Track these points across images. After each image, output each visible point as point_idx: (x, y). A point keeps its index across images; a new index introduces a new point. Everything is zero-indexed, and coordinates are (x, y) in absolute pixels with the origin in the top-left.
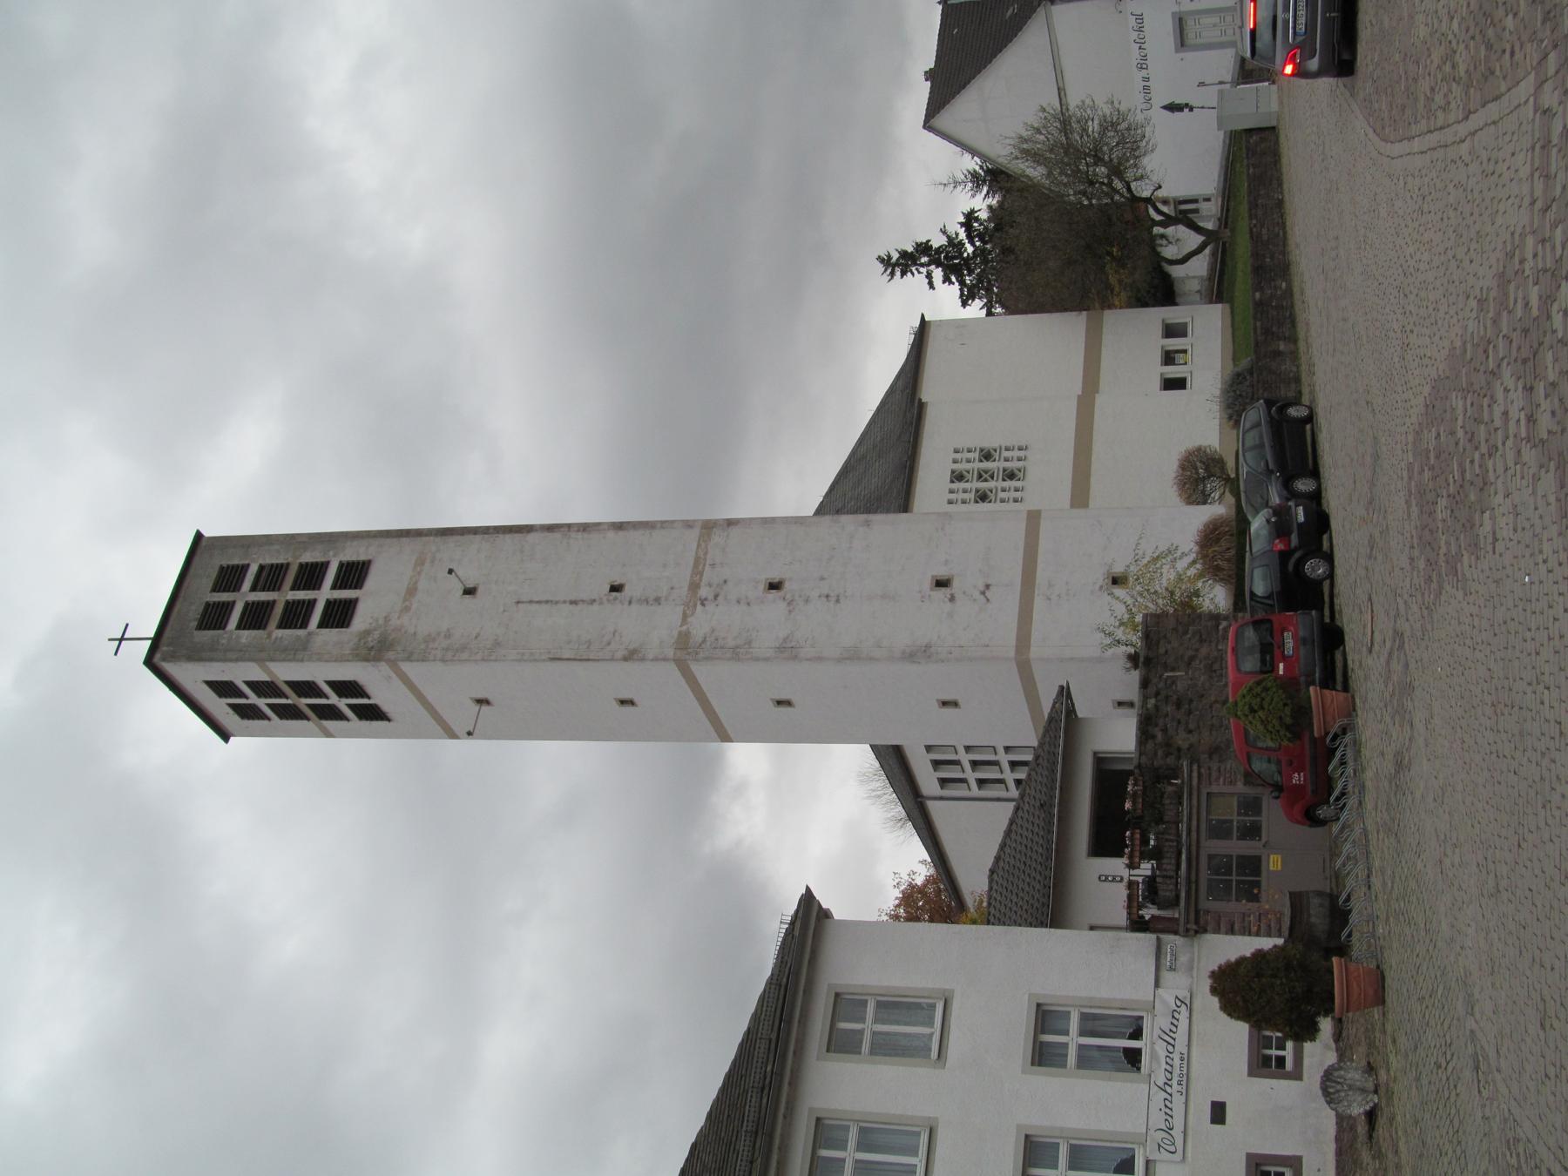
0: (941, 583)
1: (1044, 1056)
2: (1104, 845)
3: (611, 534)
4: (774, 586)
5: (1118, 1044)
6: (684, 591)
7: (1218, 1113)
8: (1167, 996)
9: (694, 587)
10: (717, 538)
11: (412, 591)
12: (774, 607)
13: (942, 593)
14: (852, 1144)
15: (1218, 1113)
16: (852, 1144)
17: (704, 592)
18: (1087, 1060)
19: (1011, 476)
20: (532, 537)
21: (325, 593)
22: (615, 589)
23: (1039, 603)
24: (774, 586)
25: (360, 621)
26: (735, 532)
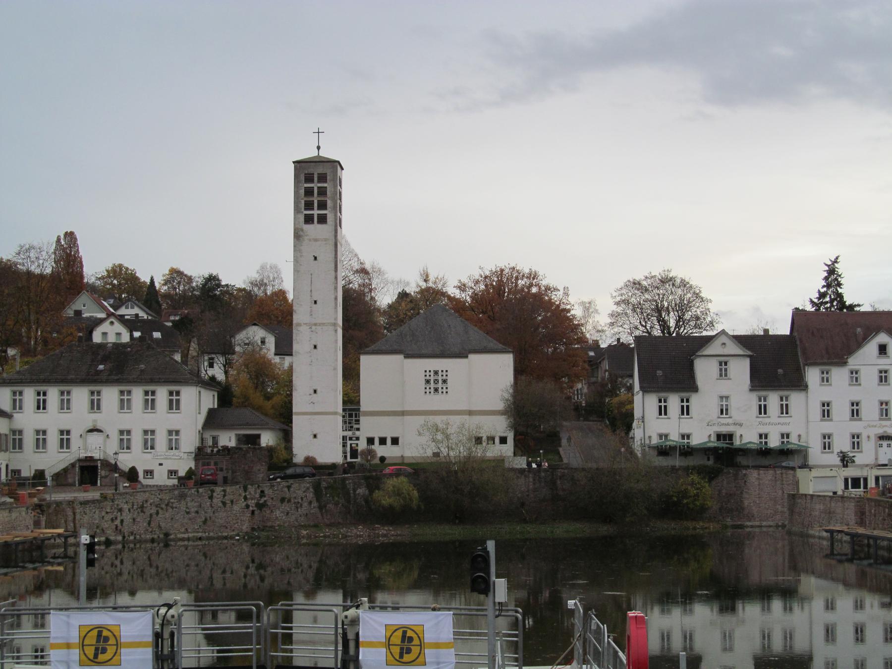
0: (315, 391)
1: (170, 432)
2: (239, 439)
3: (333, 297)
4: (315, 347)
5: (173, 446)
6: (315, 321)
7: (161, 464)
8: (182, 454)
9: (315, 325)
10: (332, 328)
11: (316, 240)
12: (308, 347)
13: (312, 392)
14: (320, 185)
15: (161, 464)
16: (320, 185)
17: (314, 327)
18: (170, 440)
19: (436, 390)
20: (333, 272)
21: (316, 212)
22: (315, 302)
23: (309, 417)
24: (315, 347)
25: (307, 227)
26: (333, 332)
